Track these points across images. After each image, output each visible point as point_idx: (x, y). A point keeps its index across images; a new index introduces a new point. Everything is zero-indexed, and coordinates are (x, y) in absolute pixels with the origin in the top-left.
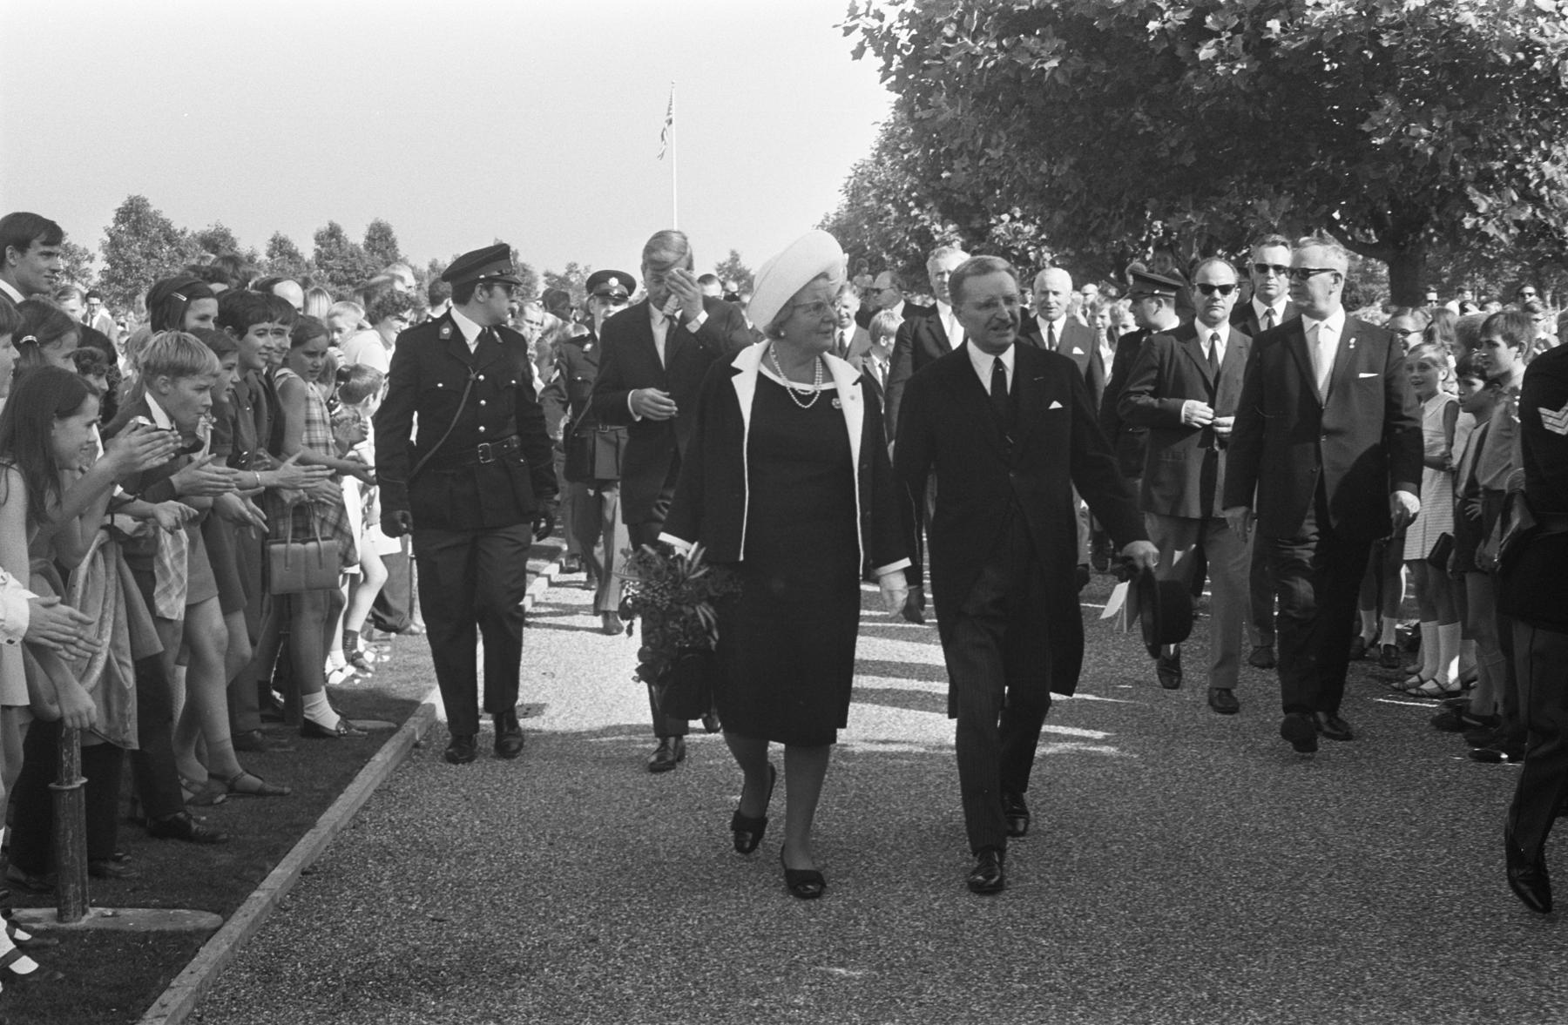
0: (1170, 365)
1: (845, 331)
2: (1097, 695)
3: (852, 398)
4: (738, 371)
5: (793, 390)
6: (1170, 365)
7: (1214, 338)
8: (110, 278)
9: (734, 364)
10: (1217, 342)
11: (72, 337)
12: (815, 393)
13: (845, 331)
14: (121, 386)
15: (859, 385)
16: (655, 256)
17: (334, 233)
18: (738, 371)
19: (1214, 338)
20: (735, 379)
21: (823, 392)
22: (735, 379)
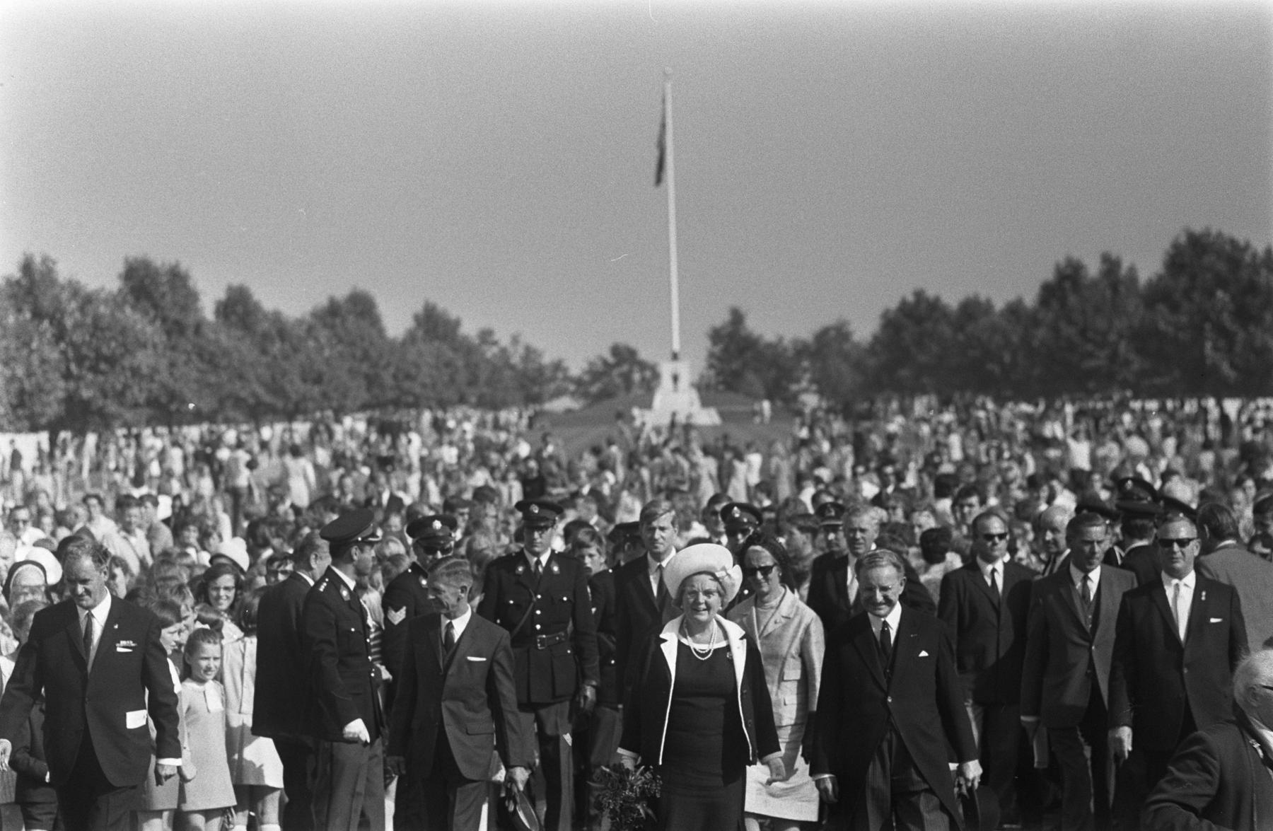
0: (965, 593)
1: (455, 622)
2: (530, 810)
3: (738, 648)
4: (664, 641)
5: (695, 650)
6: (965, 593)
7: (994, 570)
8: (598, 810)
9: (662, 636)
10: (996, 574)
11: (882, 534)
12: (710, 650)
13: (455, 622)
14: (413, 412)
15: (745, 640)
16: (1063, 447)
17: (362, 306)
18: (664, 641)
19: (994, 570)
20: (663, 646)
21: (716, 651)
22: (663, 646)
